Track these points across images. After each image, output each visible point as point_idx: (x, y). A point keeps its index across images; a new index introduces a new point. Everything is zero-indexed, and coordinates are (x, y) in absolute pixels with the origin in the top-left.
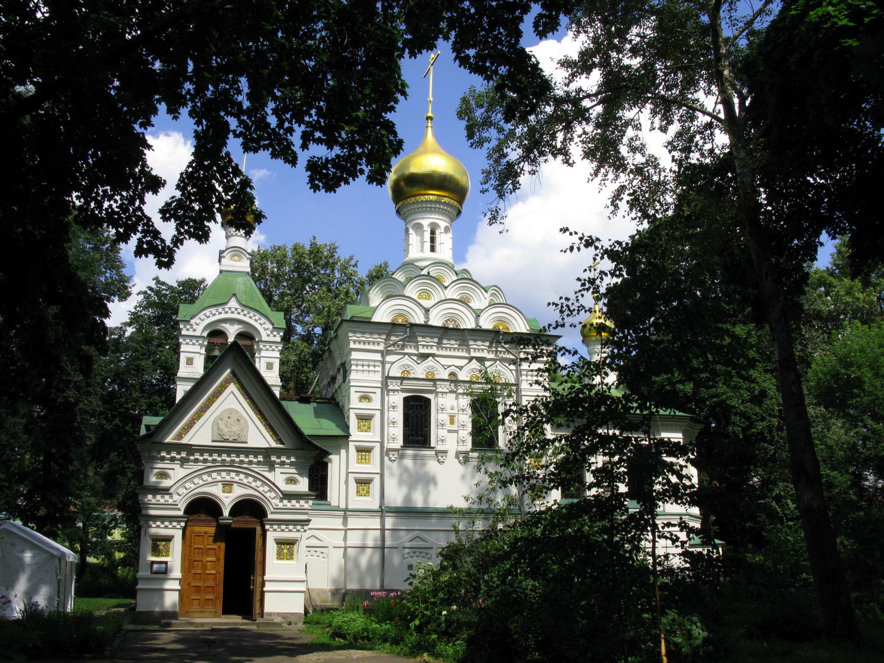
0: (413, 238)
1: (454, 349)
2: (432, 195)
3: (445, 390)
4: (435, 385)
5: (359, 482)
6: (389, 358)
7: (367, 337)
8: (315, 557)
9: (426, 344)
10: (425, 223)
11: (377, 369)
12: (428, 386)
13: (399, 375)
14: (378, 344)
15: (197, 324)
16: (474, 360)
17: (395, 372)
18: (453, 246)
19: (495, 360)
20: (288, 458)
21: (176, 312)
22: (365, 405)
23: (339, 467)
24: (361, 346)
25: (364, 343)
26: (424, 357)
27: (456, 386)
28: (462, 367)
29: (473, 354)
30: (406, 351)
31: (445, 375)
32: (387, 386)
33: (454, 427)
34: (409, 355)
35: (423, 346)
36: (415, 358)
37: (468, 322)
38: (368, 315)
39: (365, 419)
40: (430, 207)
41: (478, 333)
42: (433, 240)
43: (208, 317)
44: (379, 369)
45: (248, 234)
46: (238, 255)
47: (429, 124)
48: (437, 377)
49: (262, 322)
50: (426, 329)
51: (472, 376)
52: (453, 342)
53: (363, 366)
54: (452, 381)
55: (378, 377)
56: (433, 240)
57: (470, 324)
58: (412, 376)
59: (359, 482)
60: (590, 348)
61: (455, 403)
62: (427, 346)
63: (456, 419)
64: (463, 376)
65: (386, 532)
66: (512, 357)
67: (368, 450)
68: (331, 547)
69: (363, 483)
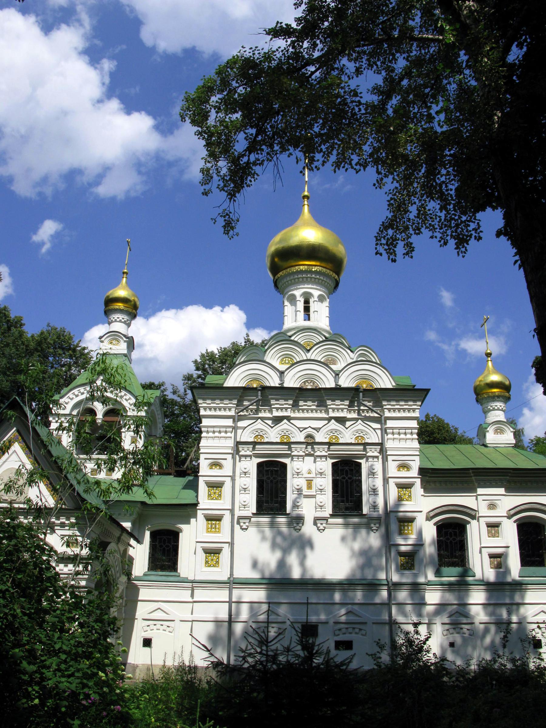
0: (288, 309)
2: (304, 265)
3: (301, 453)
4: (290, 449)
5: (207, 552)
6: (241, 424)
7: (218, 403)
8: (161, 631)
9: (280, 407)
10: (298, 293)
11: (229, 435)
12: (283, 449)
13: (251, 440)
14: (230, 410)
15: (67, 403)
16: (333, 421)
17: (246, 436)
18: (330, 314)
19: (356, 420)
20: (68, 519)
21: (201, 422)
22: (216, 471)
23: (192, 536)
24: (213, 413)
25: (215, 409)
26: (277, 420)
27: (313, 448)
28: (320, 428)
29: (332, 414)
30: (260, 415)
31: (301, 437)
32: (238, 451)
33: (312, 492)
34: (262, 419)
35: (277, 409)
36: (270, 422)
37: (328, 381)
38: (220, 382)
39: (215, 486)
40: (306, 277)
41: (338, 392)
42: (307, 309)
43: (77, 396)
44: (232, 435)
46: (113, 339)
47: (306, 203)
48: (293, 440)
49: (127, 397)
50: (282, 391)
51: (331, 438)
52: (309, 403)
53: (214, 432)
54: (307, 444)
55: (231, 443)
56: (307, 309)
57: (330, 383)
58: (266, 440)
59: (207, 552)
60: (484, 406)
61: (312, 467)
62: (404, 410)
63: (313, 483)
64: (320, 437)
65: (233, 604)
66: (376, 415)
67: (219, 519)
68: (177, 621)
69: (212, 553)
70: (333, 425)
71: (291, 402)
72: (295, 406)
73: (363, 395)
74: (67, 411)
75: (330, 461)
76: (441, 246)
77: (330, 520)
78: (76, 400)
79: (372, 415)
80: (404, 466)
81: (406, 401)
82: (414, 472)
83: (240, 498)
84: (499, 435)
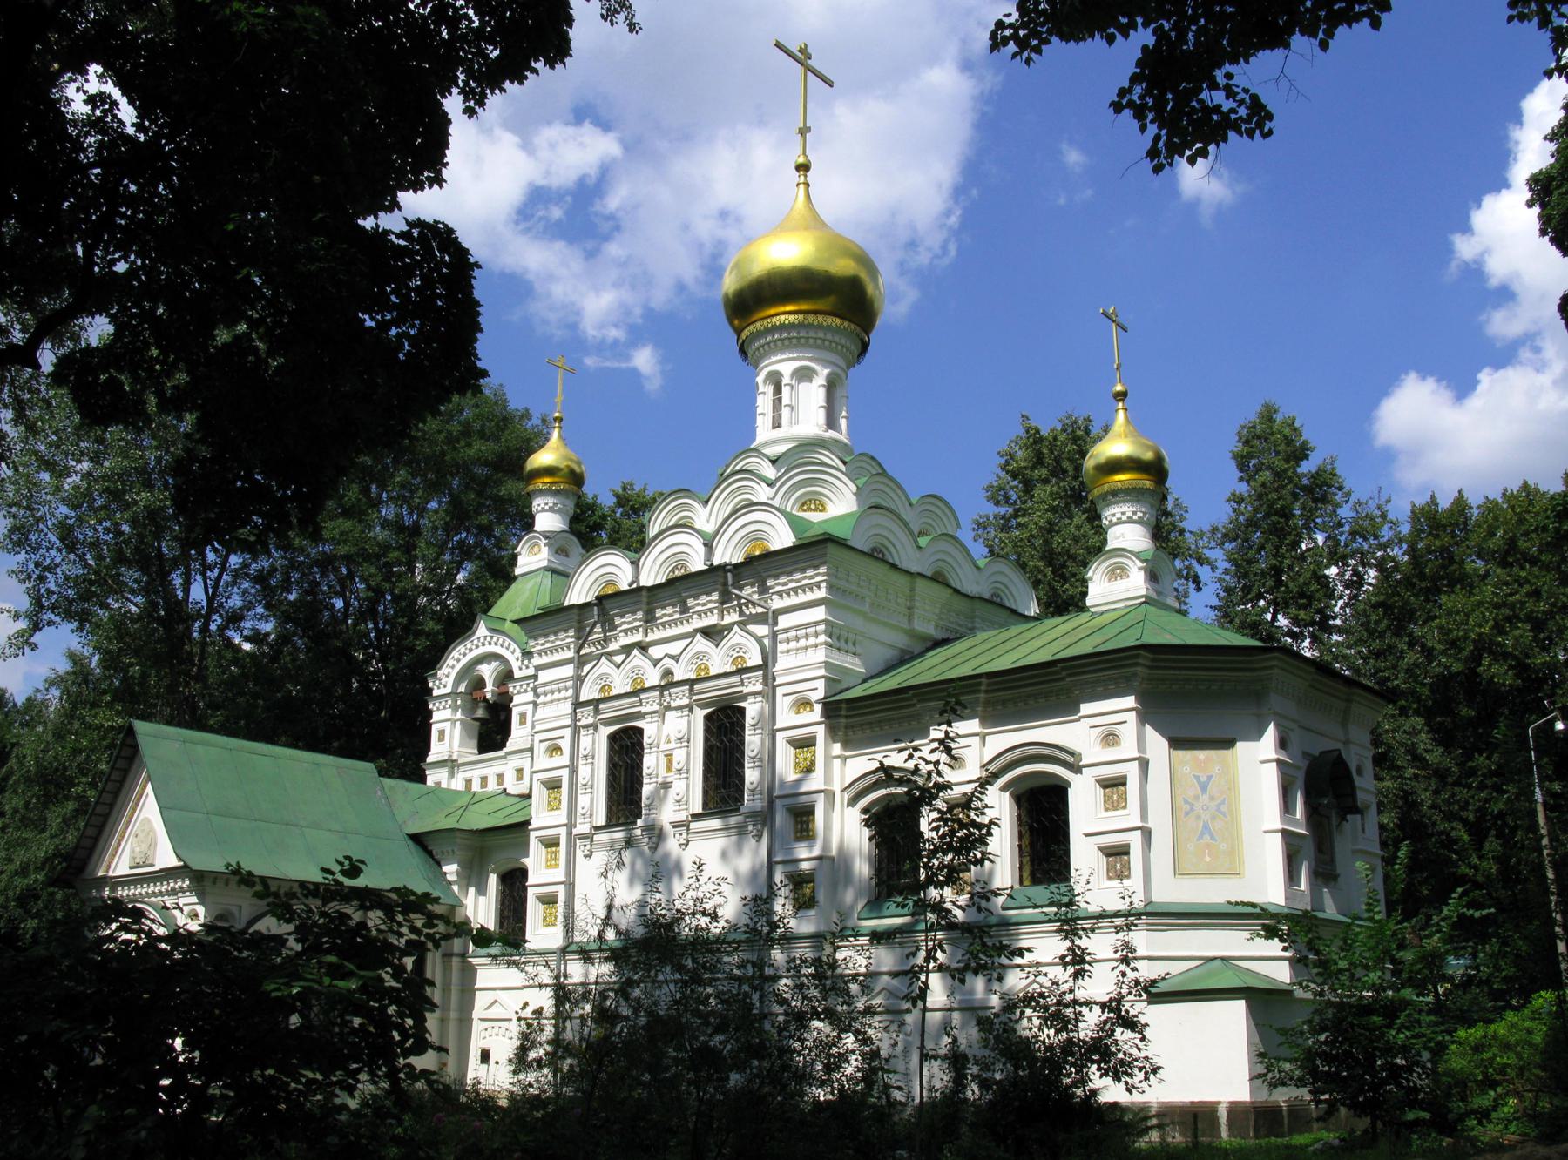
1: (675, 622)
2: (784, 315)
3: (656, 707)
17: (589, 692)
24: (793, 600)
45: (1462, 387)
52: (669, 610)
58: (615, 692)
62: (803, 588)
70: (701, 643)
71: (640, 615)
72: (650, 619)
73: (734, 576)
74: (448, 690)
75: (700, 714)
76: (1510, 19)
77: (692, 825)
78: (459, 667)
79: (753, 611)
80: (803, 704)
81: (789, 574)
82: (816, 714)
83: (583, 801)
84: (1119, 581)
